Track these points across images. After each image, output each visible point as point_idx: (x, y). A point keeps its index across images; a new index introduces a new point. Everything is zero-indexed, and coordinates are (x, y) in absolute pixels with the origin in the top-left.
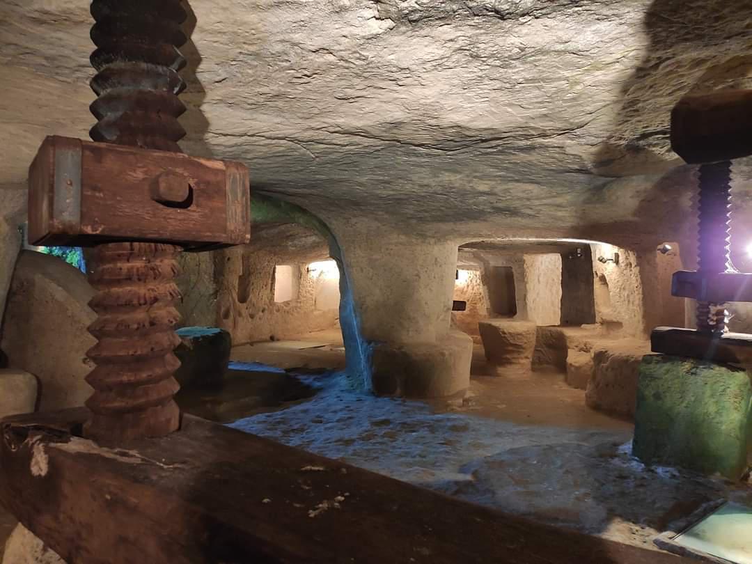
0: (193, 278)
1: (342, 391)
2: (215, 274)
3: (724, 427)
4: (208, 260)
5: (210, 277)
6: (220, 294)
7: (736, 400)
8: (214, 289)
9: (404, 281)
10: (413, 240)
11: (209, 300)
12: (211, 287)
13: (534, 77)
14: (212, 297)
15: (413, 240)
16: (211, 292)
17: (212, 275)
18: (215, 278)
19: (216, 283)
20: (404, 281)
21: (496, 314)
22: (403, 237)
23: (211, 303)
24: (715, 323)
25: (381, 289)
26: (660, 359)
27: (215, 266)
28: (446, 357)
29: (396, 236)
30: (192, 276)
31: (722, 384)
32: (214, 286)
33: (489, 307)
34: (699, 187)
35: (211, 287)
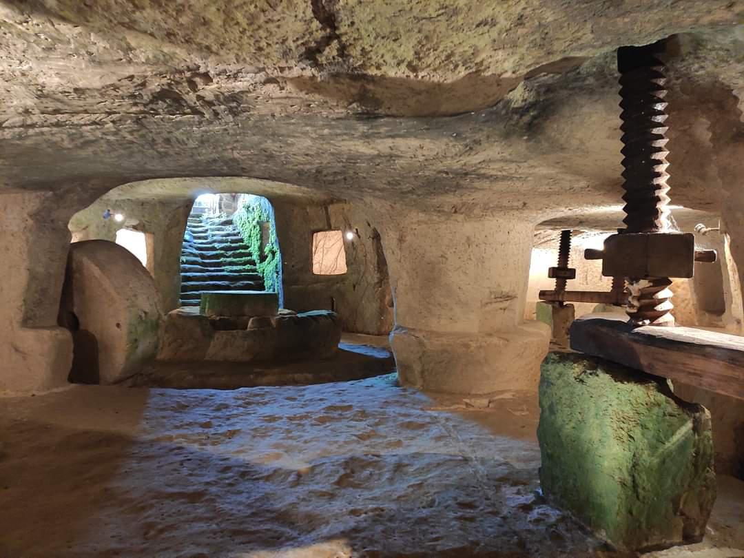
0: (362, 268)
1: (372, 386)
2: (378, 264)
3: (606, 464)
4: (372, 251)
5: (374, 267)
6: (385, 283)
7: (622, 425)
8: (378, 278)
9: (429, 264)
10: (435, 218)
11: (374, 288)
12: (376, 276)
13: (722, 17)
14: (377, 286)
15: (435, 218)
16: (376, 281)
17: (376, 265)
18: (379, 268)
19: (380, 272)
20: (429, 264)
21: (703, 312)
22: (421, 214)
23: (377, 291)
24: (635, 311)
25: (408, 272)
26: (556, 358)
27: (378, 256)
28: (472, 348)
29: (415, 214)
30: (361, 266)
31: (606, 399)
32: (378, 275)
33: (695, 303)
34: (621, 117)
35: (376, 276)
